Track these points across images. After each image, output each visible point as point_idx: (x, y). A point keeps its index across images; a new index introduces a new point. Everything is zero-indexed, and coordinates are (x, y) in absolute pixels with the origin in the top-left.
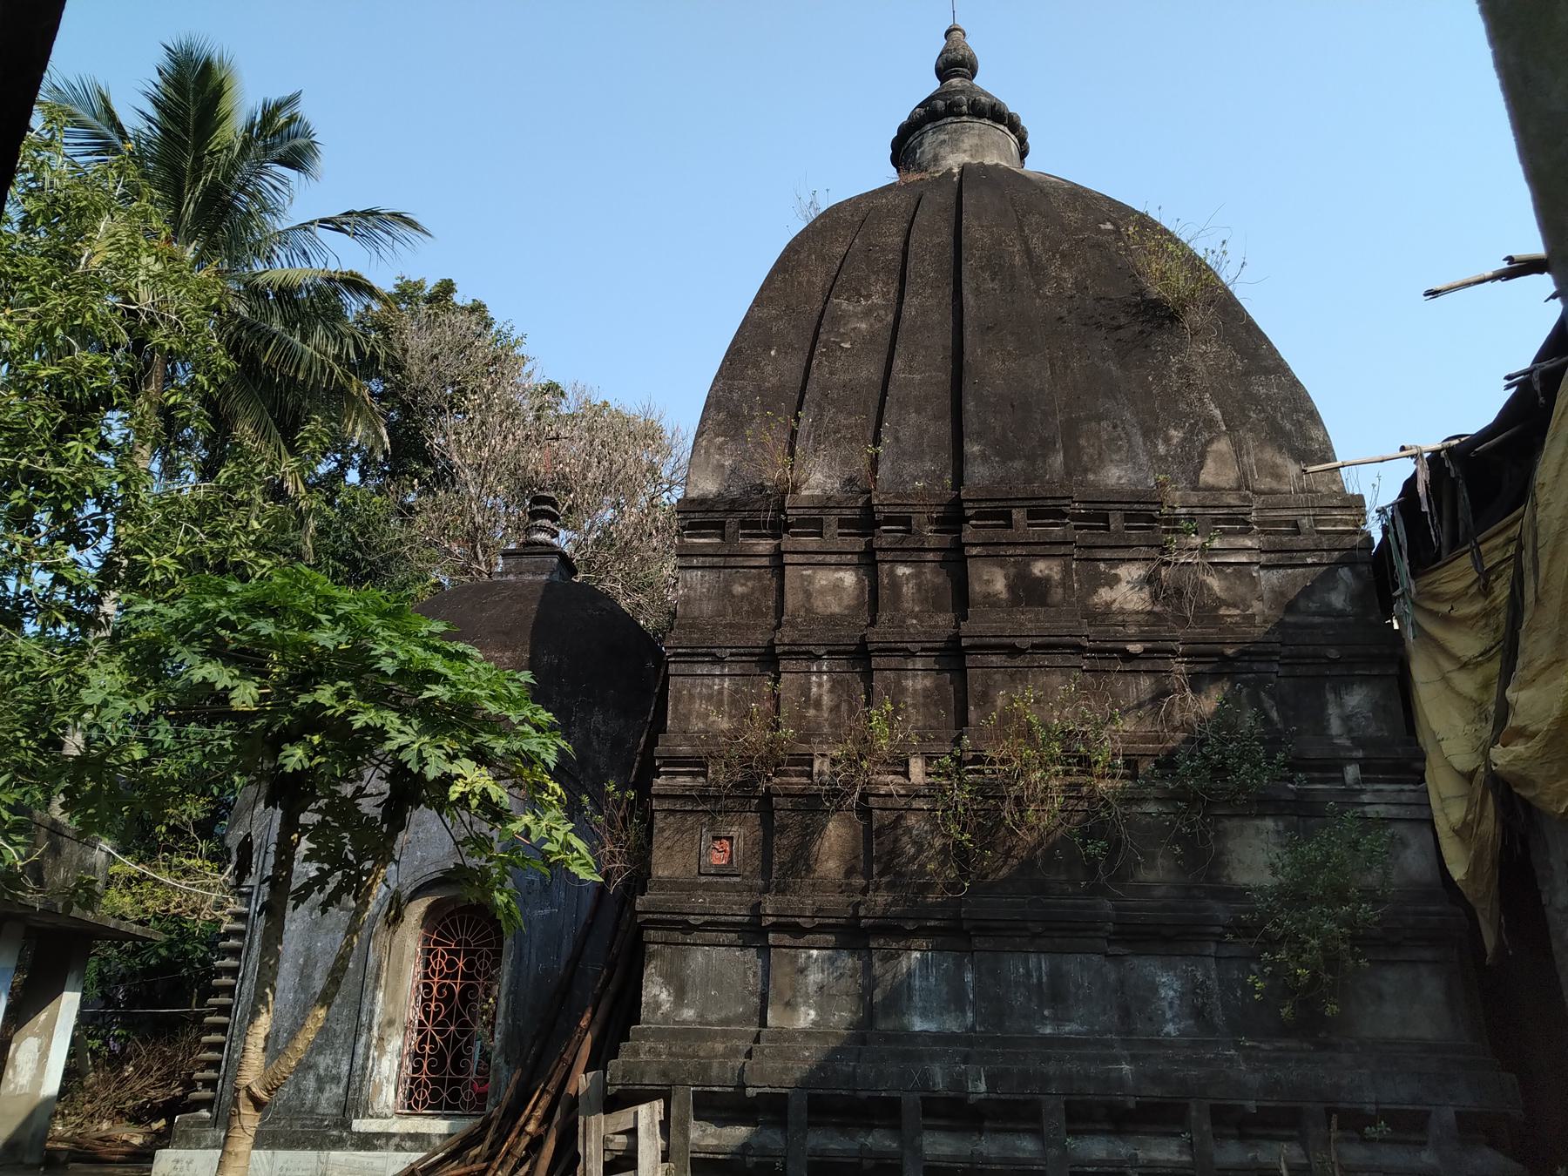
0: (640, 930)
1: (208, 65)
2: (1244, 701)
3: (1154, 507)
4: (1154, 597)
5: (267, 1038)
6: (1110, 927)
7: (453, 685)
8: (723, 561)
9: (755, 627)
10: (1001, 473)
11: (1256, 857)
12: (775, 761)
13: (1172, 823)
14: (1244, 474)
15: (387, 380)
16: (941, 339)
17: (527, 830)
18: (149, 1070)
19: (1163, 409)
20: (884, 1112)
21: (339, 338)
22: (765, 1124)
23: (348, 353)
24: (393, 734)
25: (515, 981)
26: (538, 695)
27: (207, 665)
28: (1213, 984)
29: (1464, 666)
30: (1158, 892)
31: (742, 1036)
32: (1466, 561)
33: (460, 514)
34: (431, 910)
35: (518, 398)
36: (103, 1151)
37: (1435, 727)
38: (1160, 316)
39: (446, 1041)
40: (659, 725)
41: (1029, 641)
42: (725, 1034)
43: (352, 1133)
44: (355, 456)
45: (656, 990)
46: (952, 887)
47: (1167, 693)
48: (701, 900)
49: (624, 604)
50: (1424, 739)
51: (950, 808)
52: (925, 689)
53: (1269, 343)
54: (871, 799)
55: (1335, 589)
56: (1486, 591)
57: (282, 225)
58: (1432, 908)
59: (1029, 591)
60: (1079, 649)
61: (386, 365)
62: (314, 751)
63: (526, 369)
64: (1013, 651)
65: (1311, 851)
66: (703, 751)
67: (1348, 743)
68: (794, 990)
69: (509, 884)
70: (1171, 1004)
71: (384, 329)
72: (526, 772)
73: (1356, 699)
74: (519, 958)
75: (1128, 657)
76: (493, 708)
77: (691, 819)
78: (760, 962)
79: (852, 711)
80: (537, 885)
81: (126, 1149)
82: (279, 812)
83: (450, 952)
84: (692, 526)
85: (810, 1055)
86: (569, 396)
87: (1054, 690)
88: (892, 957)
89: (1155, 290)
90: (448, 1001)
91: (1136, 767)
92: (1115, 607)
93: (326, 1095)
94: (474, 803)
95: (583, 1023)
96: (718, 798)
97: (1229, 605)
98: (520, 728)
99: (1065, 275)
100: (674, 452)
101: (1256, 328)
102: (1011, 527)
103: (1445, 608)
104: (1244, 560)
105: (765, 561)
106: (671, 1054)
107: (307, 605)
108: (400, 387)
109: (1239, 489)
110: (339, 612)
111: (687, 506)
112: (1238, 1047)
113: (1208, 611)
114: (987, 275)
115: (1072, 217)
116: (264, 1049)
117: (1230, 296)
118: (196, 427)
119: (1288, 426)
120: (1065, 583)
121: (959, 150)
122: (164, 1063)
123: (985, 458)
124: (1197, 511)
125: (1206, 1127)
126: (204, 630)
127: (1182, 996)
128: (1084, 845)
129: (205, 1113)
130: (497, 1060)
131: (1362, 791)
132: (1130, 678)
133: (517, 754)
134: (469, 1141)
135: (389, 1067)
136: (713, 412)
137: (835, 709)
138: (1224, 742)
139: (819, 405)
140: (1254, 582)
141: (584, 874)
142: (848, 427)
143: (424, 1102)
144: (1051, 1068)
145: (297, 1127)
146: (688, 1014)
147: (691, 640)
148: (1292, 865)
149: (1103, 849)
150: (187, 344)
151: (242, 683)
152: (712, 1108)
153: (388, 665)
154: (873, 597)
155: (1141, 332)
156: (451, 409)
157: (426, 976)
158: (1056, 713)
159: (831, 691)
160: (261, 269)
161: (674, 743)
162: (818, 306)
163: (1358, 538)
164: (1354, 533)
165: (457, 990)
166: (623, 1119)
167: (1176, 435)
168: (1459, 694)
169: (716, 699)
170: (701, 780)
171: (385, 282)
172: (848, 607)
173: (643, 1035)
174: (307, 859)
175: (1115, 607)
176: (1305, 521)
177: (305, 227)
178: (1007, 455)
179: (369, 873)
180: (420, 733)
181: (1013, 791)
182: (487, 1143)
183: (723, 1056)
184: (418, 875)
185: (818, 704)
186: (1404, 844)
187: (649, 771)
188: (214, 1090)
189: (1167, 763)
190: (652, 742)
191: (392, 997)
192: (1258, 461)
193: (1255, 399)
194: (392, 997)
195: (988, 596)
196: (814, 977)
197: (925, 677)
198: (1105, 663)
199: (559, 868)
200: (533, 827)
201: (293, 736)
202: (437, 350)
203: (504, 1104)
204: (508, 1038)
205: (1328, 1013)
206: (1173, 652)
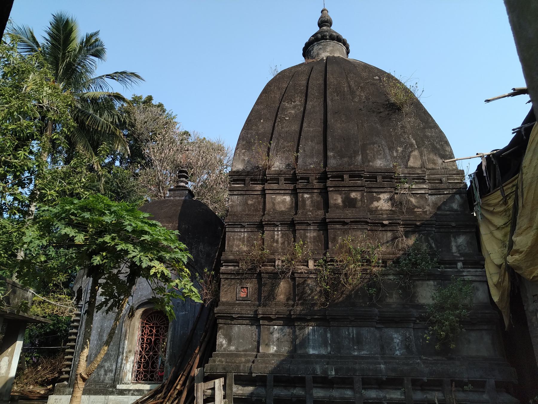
0: (216, 319)
1: (67, 21)
2: (423, 240)
4: (393, 205)
5: (87, 357)
6: (377, 318)
7: (152, 235)
8: (245, 193)
9: (256, 215)
10: (340, 162)
11: (427, 294)
12: (262, 261)
13: (399, 282)
15: (129, 130)
18: (47, 367)
19: (395, 141)
20: (300, 382)
21: (113, 116)
22: (260, 386)
24: (131, 252)
25: (173, 337)
26: (181, 238)
27: (67, 228)
29: (498, 229)
30: (394, 306)
31: (251, 356)
32: (499, 193)
33: (154, 176)
34: (144, 313)
36: (31, 396)
37: (488, 249)
38: (394, 108)
40: (223, 249)
42: (245, 355)
43: (117, 389)
44: (118, 156)
45: (221, 340)
46: (323, 304)
47: (397, 238)
48: (237, 309)
49: (211, 207)
50: (484, 254)
51: (322, 277)
52: (314, 237)
53: (432, 118)
55: (454, 202)
56: (505, 203)
57: (93, 77)
58: (487, 311)
59: (349, 203)
60: (367, 223)
61: (129, 125)
62: (103, 258)
63: (177, 127)
64: (344, 223)
65: (446, 292)
66: (238, 258)
68: (269, 340)
69: (171, 303)
70: (398, 344)
71: (128, 113)
72: (177, 265)
73: (461, 240)
74: (174, 329)
75: (383, 225)
76: (165, 243)
77: (233, 281)
79: (289, 244)
80: (181, 304)
81: (38, 395)
82: (91, 279)
83: (150, 327)
84: (234, 180)
85: (274, 362)
86: (192, 136)
87: (358, 237)
89: (393, 100)
90: (150, 344)
92: (379, 208)
93: (108, 376)
94: (159, 276)
95: (196, 351)
96: (243, 274)
97: (418, 208)
100: (228, 155)
102: (343, 181)
103: (492, 209)
104: (423, 192)
105: (259, 193)
106: (226, 362)
107: (101, 207)
108: (134, 132)
109: (421, 168)
111: (232, 174)
112: (421, 359)
113: (411, 210)
115: (364, 74)
116: (86, 361)
117: (419, 102)
118: (63, 146)
119: (438, 146)
120: (362, 200)
122: (52, 365)
123: (334, 157)
124: (407, 175)
125: (410, 386)
126: (66, 216)
127: (402, 341)
128: (368, 290)
129: (66, 383)
130: (167, 364)
131: (463, 271)
132: (384, 232)
133: (173, 259)
134: (157, 392)
135: (129, 366)
137: (283, 243)
138: (416, 255)
139: (278, 139)
140: (427, 200)
141: (196, 300)
142: (288, 147)
143: (142, 379)
144: (357, 367)
145: (98, 387)
146: (233, 348)
147: (234, 219)
150: (60, 118)
151: (78, 235)
152: (241, 380)
153: (129, 228)
154: (296, 205)
155: (388, 114)
156: (151, 140)
157: (142, 335)
158: (359, 245)
159: (282, 237)
160: (86, 92)
162: (277, 105)
163: (462, 185)
164: (461, 183)
165: (153, 340)
166: (210, 384)
167: (400, 149)
169: (242, 240)
170: (237, 268)
171: (128, 97)
172: (287, 208)
173: (217, 355)
174: (101, 295)
175: (379, 208)
176: (444, 179)
177: (101, 77)
178: (342, 157)
179: (122, 300)
180: (140, 252)
181: (344, 272)
182: (163, 393)
183: (245, 362)
184: (140, 300)
185: (277, 242)
186: (478, 289)
187: (219, 265)
188: (69, 375)
189: (397, 262)
190: (220, 255)
191: (131, 343)
193: (427, 137)
194: (131, 343)
195: (335, 204)
196: (276, 335)
197: (314, 232)
198: (376, 227)
199: (188, 298)
200: (179, 284)
201: (96, 253)
202: (146, 120)
203: (169, 379)
206: (399, 224)
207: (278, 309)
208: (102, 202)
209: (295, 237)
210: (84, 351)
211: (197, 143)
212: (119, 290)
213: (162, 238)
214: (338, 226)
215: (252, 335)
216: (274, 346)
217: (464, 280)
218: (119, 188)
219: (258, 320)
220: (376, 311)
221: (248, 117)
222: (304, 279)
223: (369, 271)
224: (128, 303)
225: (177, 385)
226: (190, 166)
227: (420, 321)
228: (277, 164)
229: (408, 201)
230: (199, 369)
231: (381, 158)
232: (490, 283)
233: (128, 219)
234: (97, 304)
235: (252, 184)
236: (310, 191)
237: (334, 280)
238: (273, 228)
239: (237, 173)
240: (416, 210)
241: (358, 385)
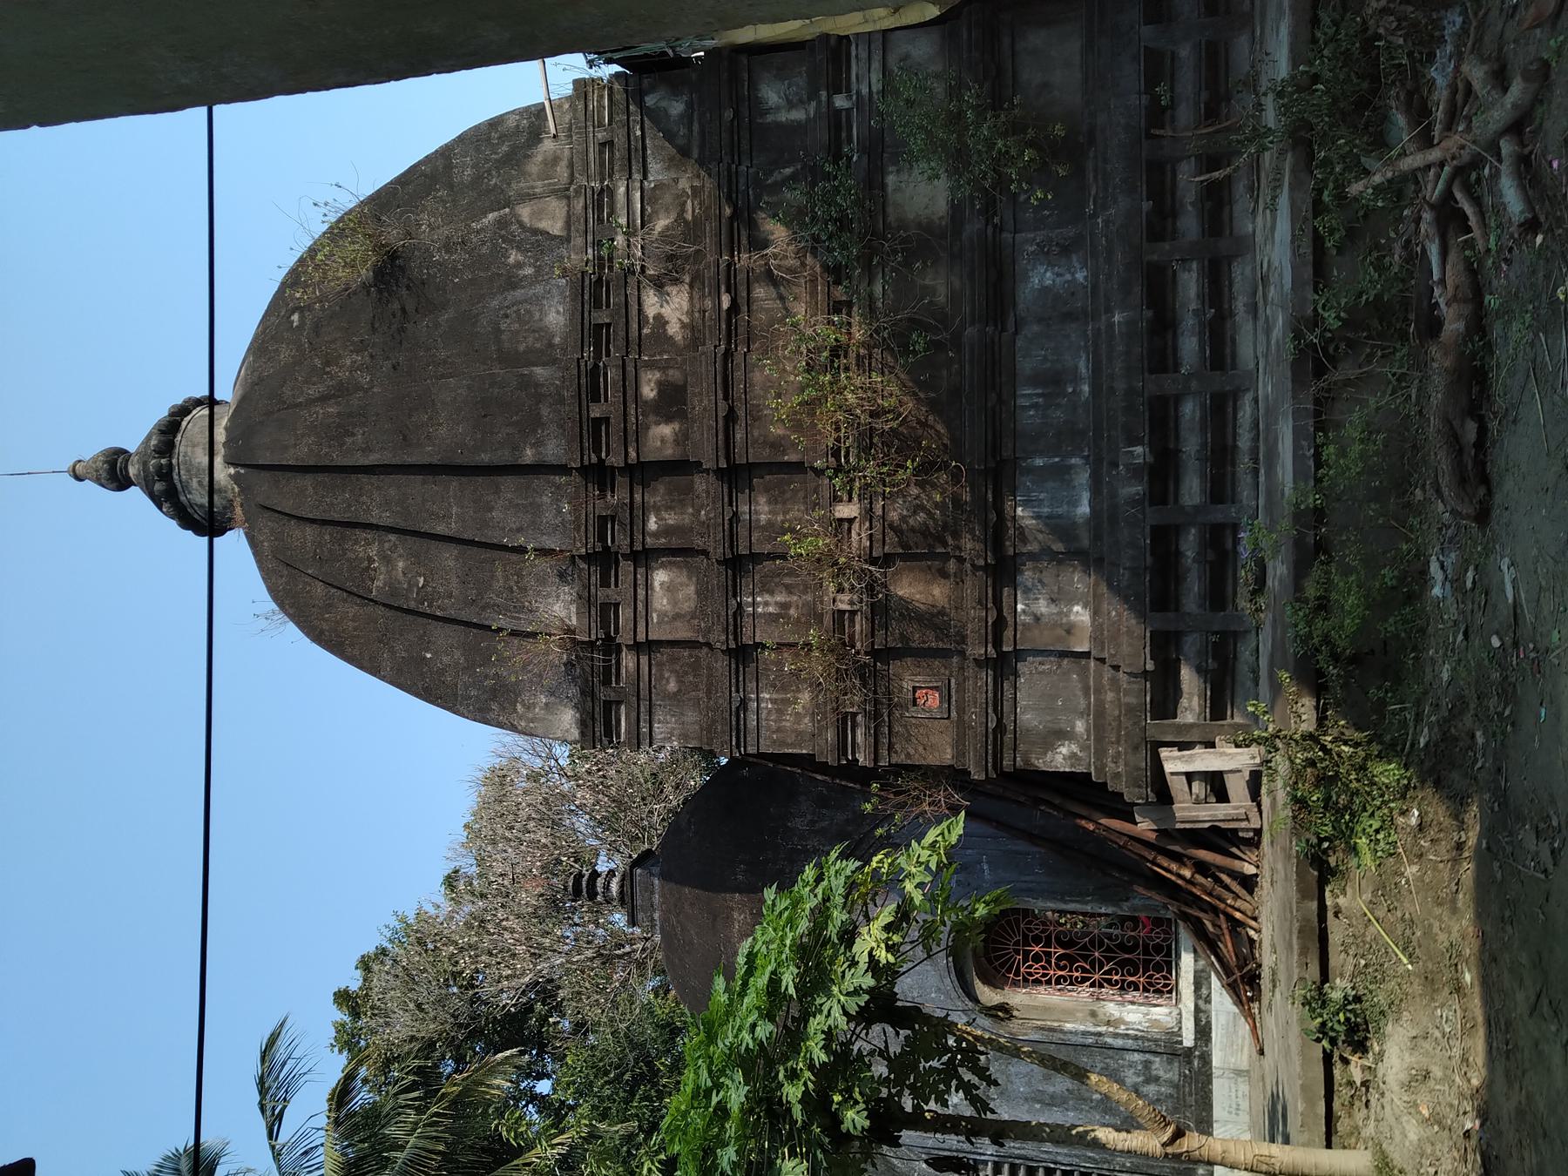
0: (1003, 775)
2: (774, 199)
3: (587, 282)
4: (676, 281)
5: (1118, 1130)
8: (644, 700)
9: (709, 668)
10: (553, 427)
11: (922, 193)
12: (840, 647)
16: (415, 486)
17: (920, 885)
19: (488, 269)
20: (1164, 540)
21: (398, 1110)
22: (1179, 649)
23: (414, 1099)
25: (1051, 894)
28: (1040, 236)
30: (957, 284)
31: (1099, 676)
33: (583, 972)
34: (987, 981)
35: (460, 919)
38: (391, 270)
39: (1109, 960)
40: (806, 761)
42: (1098, 691)
45: (1059, 758)
46: (956, 477)
48: (973, 716)
49: (675, 800)
52: (769, 502)
59: (672, 402)
60: (728, 354)
62: (849, 1100)
63: (432, 911)
64: (731, 418)
65: (917, 143)
66: (832, 717)
67: (814, 104)
68: (1056, 625)
70: (1058, 275)
71: (387, 1063)
72: (863, 889)
73: (771, 94)
74: (1030, 892)
75: (734, 308)
76: (804, 925)
77: (897, 728)
78: (1030, 659)
79: (792, 573)
80: (961, 877)
82: (904, 1133)
83: (1025, 960)
84: (608, 734)
85: (1115, 610)
88: (1022, 533)
89: (365, 273)
90: (1071, 960)
92: (686, 320)
93: (1161, 1073)
95: (1091, 827)
97: (683, 211)
99: (348, 362)
101: (403, 175)
104: (638, 194)
105: (644, 660)
106: (1118, 742)
108: (450, 1042)
109: (568, 198)
110: (709, 1084)
112: (1094, 216)
113: (691, 231)
114: (349, 440)
115: (285, 354)
120: (663, 369)
123: (539, 444)
124: (590, 238)
125: (1167, 246)
127: (1051, 265)
128: (915, 352)
130: (1125, 909)
131: (858, 93)
134: (1200, 933)
135: (1135, 1015)
137: (789, 589)
139: (484, 608)
141: (959, 830)
142: (507, 579)
143: (1165, 978)
144: (1120, 385)
145: (1191, 1100)
146: (1080, 726)
148: (929, 160)
152: (1165, 701)
154: (680, 553)
155: (408, 287)
156: (473, 987)
157: (1049, 982)
159: (772, 593)
161: (824, 746)
162: (380, 610)
163: (616, 86)
164: (611, 89)
165: (1062, 951)
166: (1177, 786)
167: (514, 257)
169: (781, 706)
170: (859, 718)
172: (690, 578)
173: (1101, 769)
174: (945, 1104)
175: (686, 320)
176: (599, 136)
177: (276, 1155)
178: (535, 422)
179: (959, 1040)
180: (829, 995)
183: (1118, 691)
184: (954, 995)
185: (785, 606)
186: (906, 57)
187: (851, 770)
189: (836, 273)
190: (823, 768)
191: (1069, 1014)
192: (540, 179)
193: (477, 180)
194: (1069, 1014)
195: (677, 442)
196: (1043, 607)
197: (757, 503)
199: (951, 852)
200: (917, 880)
201: (833, 1122)
202: (412, 1006)
203: (1167, 901)
204: (1105, 900)
206: (729, 266)
207: (969, 603)
208: (685, 1114)
209: (772, 557)
210: (1104, 1140)
213: (790, 935)
216: (1070, 611)
217: (883, 92)
218: (619, 1077)
219: (1002, 656)
220: (970, 331)
223: (862, 351)
225: (1180, 876)
227: (995, 214)
228: (558, 609)
231: (541, 310)
233: (736, 1036)
234: (968, 1111)
235: (617, 682)
239: (584, 724)
241: (1168, 384)
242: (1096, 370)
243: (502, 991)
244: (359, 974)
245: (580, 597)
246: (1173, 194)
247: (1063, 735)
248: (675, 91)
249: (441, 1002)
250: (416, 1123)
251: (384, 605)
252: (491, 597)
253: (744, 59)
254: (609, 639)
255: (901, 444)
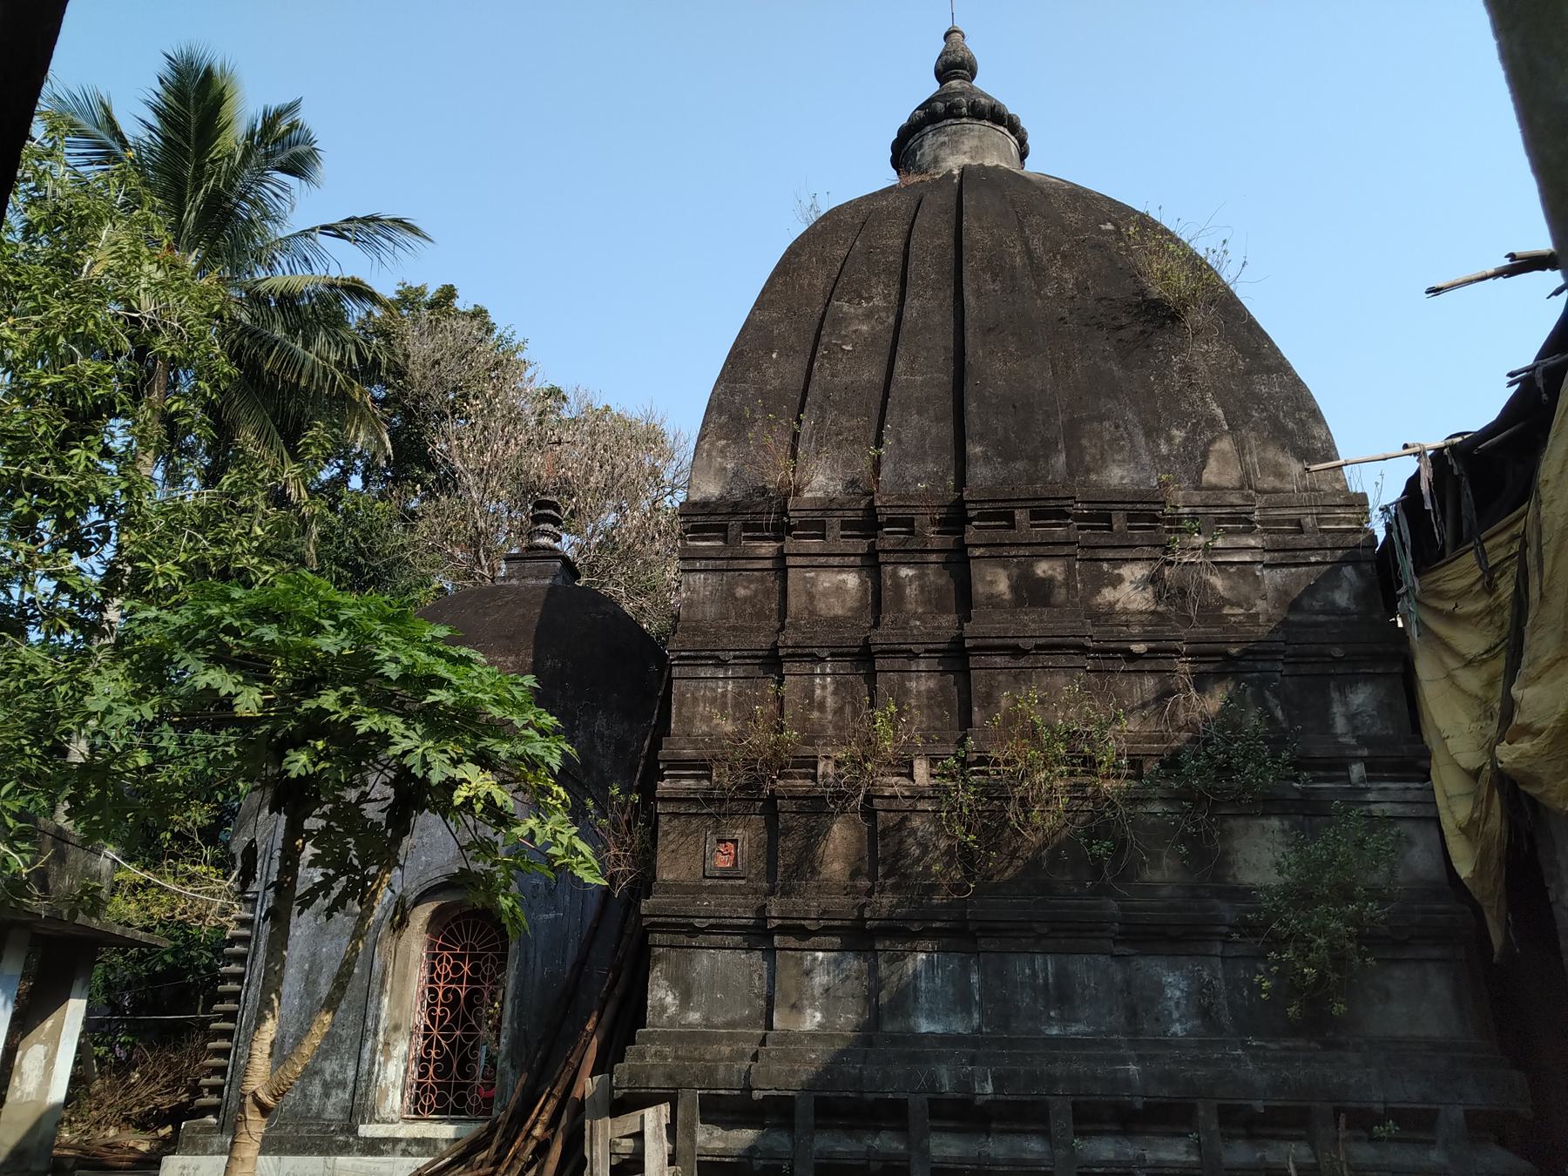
1: (209, 72)
2: (1249, 699)
4: (1158, 597)
5: (273, 1044)
7: (457, 690)
8: (728, 565)
9: (759, 629)
10: (1004, 473)
11: (1262, 857)
12: (779, 763)
14: (1247, 474)
15: (389, 386)
19: (1165, 408)
20: (891, 1114)
21: (341, 344)
23: (350, 360)
24: (397, 738)
27: (211, 672)
29: (1469, 664)
30: (1164, 892)
31: (748, 1039)
32: (1470, 558)
33: (463, 519)
34: (436, 915)
36: (110, 1158)
37: (1440, 724)
38: (1161, 316)
40: (663, 728)
41: (1033, 642)
42: (731, 1037)
44: (358, 462)
45: (661, 994)
46: (957, 888)
48: (706, 903)
49: (628, 607)
50: (1430, 737)
52: (929, 691)
53: (1271, 342)
54: (875, 801)
55: (1338, 587)
56: (1490, 588)
59: (1032, 592)
60: (1083, 650)
61: (388, 371)
62: (318, 757)
63: (528, 374)
64: (1017, 652)
65: (1317, 850)
66: (707, 754)
67: (1353, 742)
68: (801, 993)
70: (1177, 1004)
71: (386, 335)
72: (530, 776)
73: (1361, 697)
74: (525, 961)
75: (1132, 657)
77: (695, 822)
79: (856, 712)
81: (132, 1156)
82: (284, 817)
83: (455, 956)
84: (695, 529)
85: (816, 1057)
86: (571, 400)
88: (898, 959)
89: (1156, 291)
90: (453, 1005)
91: (1141, 766)
92: (1118, 607)
93: (333, 1100)
94: (479, 807)
95: (589, 1027)
96: (722, 801)
97: (1232, 605)
98: (524, 732)
100: (676, 455)
102: (1013, 527)
104: (1248, 559)
105: (768, 564)
106: (677, 1058)
107: (310, 610)
108: (402, 393)
109: (1242, 488)
111: (690, 510)
112: (1245, 1046)
113: (1212, 611)
115: (1072, 217)
116: (270, 1055)
117: (1232, 296)
118: (198, 435)
120: (1068, 583)
121: (959, 152)
122: (170, 1069)
123: (987, 459)
124: (1200, 510)
125: (1214, 1127)
126: (208, 637)
127: (1188, 996)
128: (1090, 845)
130: (503, 1064)
131: (1368, 790)
133: (520, 758)
134: (476, 1145)
135: (395, 1072)
136: (715, 416)
137: (839, 711)
139: (821, 407)
141: (588, 878)
144: (1058, 1069)
145: (303, 1132)
146: (694, 1017)
148: (1298, 864)
149: (1108, 849)
150: (189, 351)
151: (246, 689)
152: (718, 1111)
153: (392, 671)
154: (877, 599)
155: (1143, 332)
156: (453, 414)
157: (432, 981)
158: (1060, 714)
159: (835, 693)
162: (819, 309)
163: (1362, 537)
164: (1358, 531)
165: (463, 994)
166: (629, 1122)
167: (1178, 434)
168: (1464, 692)
169: (720, 702)
170: (706, 783)
171: (387, 289)
172: (851, 609)
173: (650, 1038)
174: (312, 864)
175: (1118, 607)
176: (1308, 519)
177: (306, 234)
178: (1008, 456)
179: (373, 878)
180: (423, 738)
181: (1018, 792)
182: (494, 1147)
183: (731, 1059)
184: (423, 880)
185: (822, 706)
186: (1411, 842)
187: (653, 774)
189: (1172, 763)
190: (656, 746)
191: (398, 1002)
193: (1257, 398)
194: (398, 1002)
196: (820, 979)
199: (564, 872)
200: (537, 831)
201: (298, 743)
202: (438, 356)
203: (510, 1109)
204: (514, 1041)
205: (1335, 1011)
206: (1176, 651)
207: (825, 901)
210: (263, 1028)
211: (586, 420)
212: (364, 850)
214: (999, 661)
215: (751, 978)
217: (1370, 816)
219: (769, 935)
220: (1113, 905)
221: (735, 345)
222: (901, 815)
223: (1090, 789)
224: (389, 885)
226: (566, 488)
228: (819, 480)
229: (1205, 586)
230: (596, 1078)
232: (1448, 824)
234: (300, 889)
236: (917, 558)
237: (988, 818)
238: (808, 666)
240: (1226, 611)
242: (1074, 1043)
243: (447, 440)
244: (470, 308)
245: (831, 501)
246: (1273, 1137)
247: (685, 1000)
248: (1360, 597)
249: (440, 382)
250: (327, 360)
251: (824, 313)
252: (831, 415)
253: (1398, 669)
254: (790, 529)
255: (993, 829)
